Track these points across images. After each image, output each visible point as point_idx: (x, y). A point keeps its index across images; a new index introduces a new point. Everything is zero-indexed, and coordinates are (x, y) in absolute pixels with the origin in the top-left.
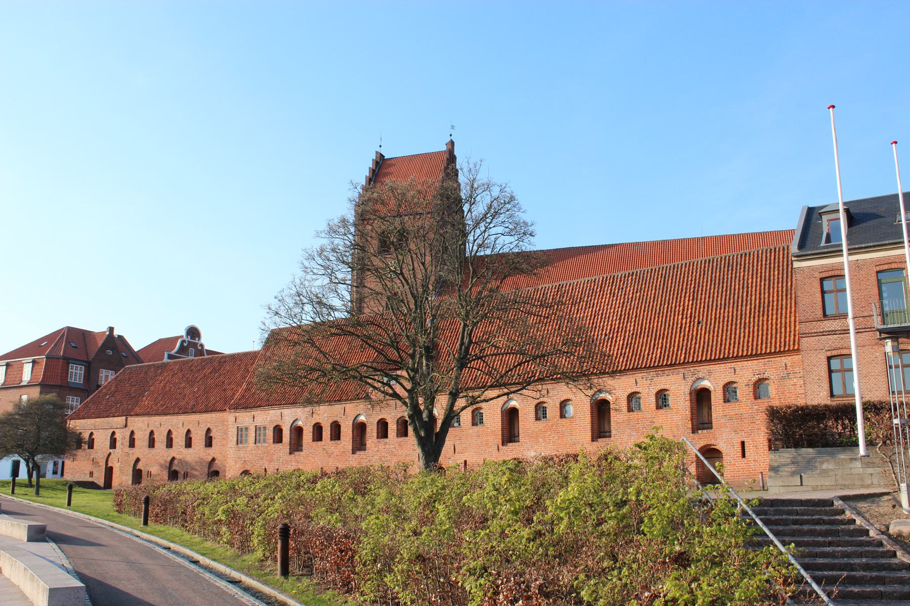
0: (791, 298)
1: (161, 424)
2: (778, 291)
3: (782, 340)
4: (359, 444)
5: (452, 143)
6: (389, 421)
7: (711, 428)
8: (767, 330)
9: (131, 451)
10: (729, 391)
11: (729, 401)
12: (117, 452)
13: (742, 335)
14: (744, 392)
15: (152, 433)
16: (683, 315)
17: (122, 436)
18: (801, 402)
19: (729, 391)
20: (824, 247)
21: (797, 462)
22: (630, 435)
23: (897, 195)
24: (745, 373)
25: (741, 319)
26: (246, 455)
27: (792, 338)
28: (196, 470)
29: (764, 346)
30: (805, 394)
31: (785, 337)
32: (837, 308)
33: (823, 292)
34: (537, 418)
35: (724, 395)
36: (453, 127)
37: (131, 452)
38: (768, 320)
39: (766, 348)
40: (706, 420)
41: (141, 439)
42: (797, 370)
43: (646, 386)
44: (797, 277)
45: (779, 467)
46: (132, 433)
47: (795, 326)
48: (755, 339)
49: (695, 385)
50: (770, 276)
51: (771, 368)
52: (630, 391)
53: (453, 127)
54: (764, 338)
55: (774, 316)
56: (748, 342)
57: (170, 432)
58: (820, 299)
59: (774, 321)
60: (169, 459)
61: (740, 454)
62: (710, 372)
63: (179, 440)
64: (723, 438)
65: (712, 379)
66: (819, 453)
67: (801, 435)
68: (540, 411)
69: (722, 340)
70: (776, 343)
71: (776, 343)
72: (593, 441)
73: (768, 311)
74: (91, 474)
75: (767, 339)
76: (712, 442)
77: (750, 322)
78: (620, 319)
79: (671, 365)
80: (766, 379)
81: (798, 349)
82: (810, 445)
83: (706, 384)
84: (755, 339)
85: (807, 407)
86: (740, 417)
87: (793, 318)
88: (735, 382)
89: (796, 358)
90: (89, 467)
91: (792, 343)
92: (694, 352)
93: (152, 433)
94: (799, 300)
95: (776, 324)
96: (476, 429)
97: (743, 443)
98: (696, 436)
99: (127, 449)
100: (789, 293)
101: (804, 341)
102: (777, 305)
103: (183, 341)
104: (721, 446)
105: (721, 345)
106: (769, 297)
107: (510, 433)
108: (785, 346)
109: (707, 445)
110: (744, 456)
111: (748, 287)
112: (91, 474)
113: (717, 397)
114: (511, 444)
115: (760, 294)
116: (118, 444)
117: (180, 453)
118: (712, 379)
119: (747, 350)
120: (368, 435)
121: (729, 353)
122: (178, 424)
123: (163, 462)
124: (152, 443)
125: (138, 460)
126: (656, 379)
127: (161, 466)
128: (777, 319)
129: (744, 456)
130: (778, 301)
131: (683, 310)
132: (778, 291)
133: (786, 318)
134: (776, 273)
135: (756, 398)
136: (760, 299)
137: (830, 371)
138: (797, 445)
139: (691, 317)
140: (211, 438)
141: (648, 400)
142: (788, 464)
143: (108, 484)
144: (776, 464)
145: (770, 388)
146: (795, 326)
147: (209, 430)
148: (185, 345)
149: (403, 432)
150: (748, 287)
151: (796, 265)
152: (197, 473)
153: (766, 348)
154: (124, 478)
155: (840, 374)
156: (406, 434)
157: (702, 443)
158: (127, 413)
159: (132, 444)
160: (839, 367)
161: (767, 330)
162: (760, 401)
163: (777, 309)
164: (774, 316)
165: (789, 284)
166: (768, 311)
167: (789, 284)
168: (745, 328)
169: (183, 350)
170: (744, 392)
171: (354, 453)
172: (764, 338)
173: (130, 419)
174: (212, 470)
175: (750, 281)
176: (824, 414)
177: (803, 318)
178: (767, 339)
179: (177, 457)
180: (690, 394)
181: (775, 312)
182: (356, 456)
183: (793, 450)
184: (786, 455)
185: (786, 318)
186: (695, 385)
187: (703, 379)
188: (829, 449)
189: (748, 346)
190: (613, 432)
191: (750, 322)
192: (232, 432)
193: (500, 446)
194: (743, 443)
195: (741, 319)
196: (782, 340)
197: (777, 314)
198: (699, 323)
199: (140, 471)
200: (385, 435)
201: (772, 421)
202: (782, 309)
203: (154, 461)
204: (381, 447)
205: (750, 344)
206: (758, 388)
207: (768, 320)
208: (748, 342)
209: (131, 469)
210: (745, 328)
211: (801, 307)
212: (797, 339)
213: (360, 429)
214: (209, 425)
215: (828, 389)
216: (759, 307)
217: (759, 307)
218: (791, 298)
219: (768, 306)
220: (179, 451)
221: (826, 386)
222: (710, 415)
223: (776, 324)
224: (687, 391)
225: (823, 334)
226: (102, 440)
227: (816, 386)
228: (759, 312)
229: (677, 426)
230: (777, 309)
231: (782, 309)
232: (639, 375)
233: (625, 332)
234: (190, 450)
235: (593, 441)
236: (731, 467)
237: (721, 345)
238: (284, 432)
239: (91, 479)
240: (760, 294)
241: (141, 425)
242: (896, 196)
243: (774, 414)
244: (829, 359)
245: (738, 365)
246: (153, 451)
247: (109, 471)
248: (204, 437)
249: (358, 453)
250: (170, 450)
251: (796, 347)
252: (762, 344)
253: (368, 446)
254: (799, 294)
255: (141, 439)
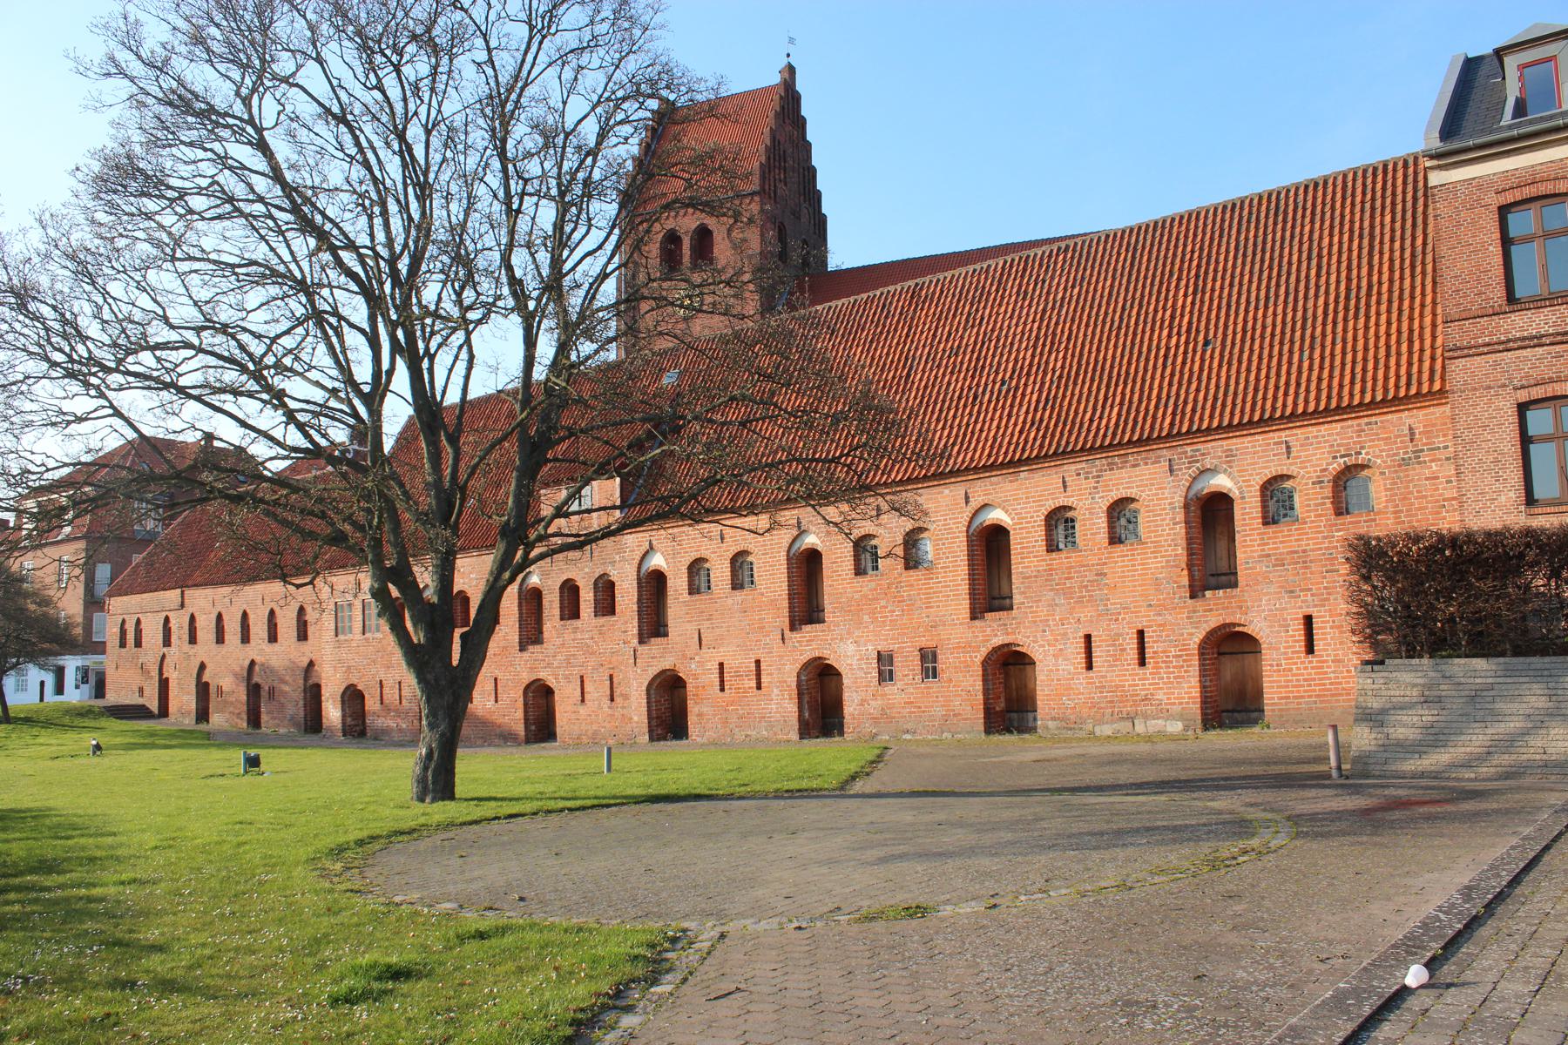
0: (1424, 273)
2: (1391, 260)
3: (1403, 371)
5: (791, 70)
6: (580, 583)
7: (1235, 585)
8: (1366, 349)
9: (192, 650)
10: (1276, 499)
11: (1275, 522)
12: (173, 652)
13: (1306, 365)
14: (1310, 499)
15: (220, 617)
16: (1171, 327)
17: (179, 623)
18: (1449, 523)
19: (1276, 499)
20: (1510, 127)
21: (1439, 700)
22: (1053, 605)
24: (1312, 453)
25: (1303, 328)
26: (350, 656)
27: (1426, 365)
28: (286, 682)
29: (1358, 387)
30: (1460, 499)
31: (1410, 364)
32: (1546, 279)
33: (1506, 242)
34: (859, 571)
35: (1264, 506)
36: (792, 41)
38: (1367, 328)
39: (1363, 392)
40: (1223, 565)
42: (1439, 441)
43: (1087, 490)
44: (1440, 207)
45: (1383, 711)
46: (192, 618)
47: (1434, 338)
48: (1337, 373)
49: (1197, 487)
50: (1372, 227)
51: (1376, 440)
52: (1051, 504)
53: (792, 41)
54: (1359, 368)
55: (1383, 318)
56: (1320, 379)
57: (245, 615)
58: (1497, 259)
59: (1383, 329)
60: (247, 663)
61: (1300, 646)
62: (1230, 455)
64: (1262, 609)
65: (1236, 470)
66: (1509, 672)
67: (1451, 620)
68: (864, 554)
69: (1257, 379)
70: (1386, 378)
71: (1386, 378)
72: (973, 618)
73: (1368, 306)
74: (141, 690)
75: (1364, 370)
76: (1237, 618)
77: (1324, 335)
78: (1035, 347)
79: (1140, 442)
80: (1363, 467)
81: (1442, 391)
82: (1481, 647)
83: (1221, 482)
84: (1337, 373)
85: (1470, 537)
86: (1301, 559)
87: (1428, 320)
88: (1289, 477)
89: (1438, 412)
90: (136, 680)
91: (1425, 376)
92: (1194, 410)
93: (220, 617)
94: (1444, 264)
95: (1388, 335)
96: (739, 596)
97: (1308, 620)
98: (1198, 604)
99: (186, 647)
100: (1421, 262)
101: (1460, 371)
102: (1390, 291)
104: (1256, 626)
105: (1256, 390)
106: (1370, 275)
107: (806, 605)
108: (1408, 384)
109: (1224, 626)
110: (1310, 649)
111: (1320, 256)
112: (141, 690)
113: (1247, 513)
114: (808, 628)
115: (1349, 269)
116: (174, 638)
118: (1236, 470)
119: (1318, 399)
120: (546, 613)
121: (1274, 409)
123: (237, 669)
125: (202, 667)
126: (1107, 475)
127: (236, 675)
128: (1389, 323)
129: (1310, 649)
130: (1391, 281)
131: (1172, 317)
132: (1391, 260)
133: (1411, 319)
134: (1388, 219)
135: (1339, 512)
136: (1349, 279)
137: (1526, 441)
138: (1440, 645)
139: (1188, 331)
141: (1092, 524)
142: (1411, 706)
143: (164, 712)
144: (1375, 704)
145: (1372, 487)
146: (1434, 338)
150: (1320, 256)
151: (1435, 178)
152: (287, 688)
153: (1363, 392)
154: (185, 698)
155: (1552, 446)
157: (1213, 621)
158: (183, 584)
159: (193, 639)
160: (1549, 429)
161: (1366, 349)
162: (1348, 518)
163: (1390, 301)
164: (1383, 318)
165: (1419, 241)
166: (1368, 306)
167: (1419, 241)
168: (1312, 348)
170: (1310, 499)
171: (522, 649)
172: (1359, 368)
173: (188, 592)
174: (311, 682)
175: (1326, 241)
176: (1521, 556)
177: (1454, 312)
178: (1364, 370)
179: (258, 659)
180: (1186, 506)
181: (1383, 308)
182: (526, 655)
183: (1425, 661)
184: (1407, 677)
185: (1411, 319)
186: (1197, 487)
187: (1213, 471)
188: (1537, 661)
189: (1319, 390)
190: (1017, 599)
191: (1324, 335)
193: (787, 632)
194: (1308, 620)
195: (1303, 328)
196: (1403, 371)
197: (1389, 311)
198: (1206, 343)
199: (207, 684)
200: (575, 615)
201: (1367, 578)
202: (1401, 299)
203: (227, 666)
204: (568, 636)
205: (1324, 384)
206: (1345, 484)
207: (1367, 328)
208: (1320, 379)
209: (194, 683)
210: (1312, 348)
211: (1447, 285)
212: (1438, 366)
215: (1520, 485)
216: (1347, 298)
217: (1347, 298)
218: (1424, 273)
219: (1369, 295)
220: (259, 648)
221: (1515, 476)
222: (1232, 554)
223: (1388, 335)
224: (1179, 500)
225: (1506, 346)
227: (1489, 479)
228: (1346, 309)
229: (1157, 583)
230: (1390, 301)
231: (1401, 299)
232: (1070, 469)
233: (1045, 373)
234: (276, 647)
235: (973, 618)
236: (1282, 675)
237: (1256, 390)
238: (582, 593)
239: (140, 701)
240: (1349, 269)
241: (205, 602)
243: (1370, 558)
244: (1522, 408)
245: (1297, 436)
247: (164, 685)
249: (531, 648)
250: (248, 647)
251: (1437, 386)
252: (1352, 383)
253: (546, 635)
254: (1443, 250)
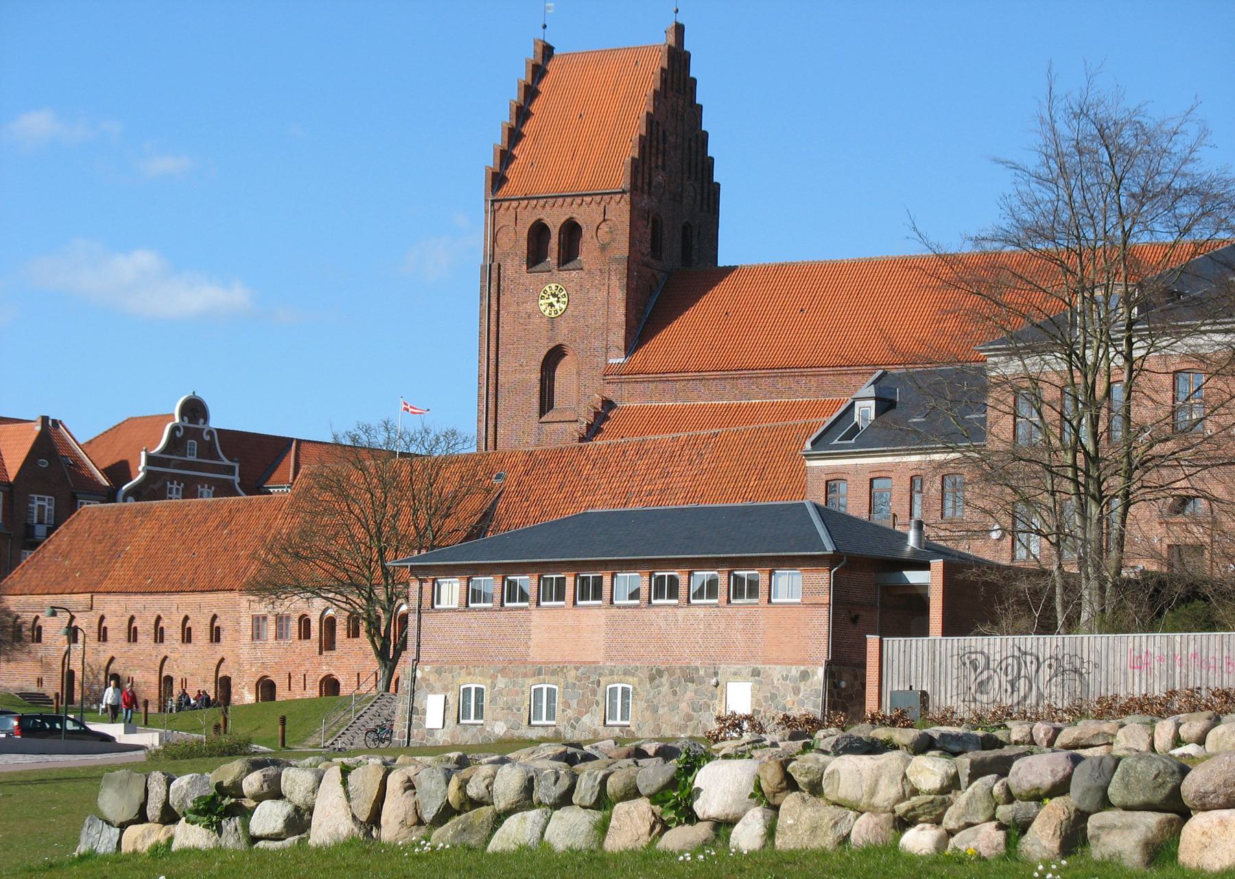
1: (146, 608)
4: (328, 643)
5: (679, 30)
23: (947, 631)
37: (102, 648)
41: (116, 627)
63: (173, 632)
74: (40, 681)
103: (175, 429)
112: (40, 681)
117: (174, 650)
122: (173, 608)
124: (132, 635)
140: (218, 628)
147: (159, 618)
148: (179, 434)
149: (354, 633)
156: (356, 635)
169: (175, 443)
174: (220, 675)
192: (246, 623)
213: (329, 625)
214: (215, 611)
226: (54, 629)
241: (115, 609)
242: (947, 631)
246: (135, 647)
248: (208, 627)
250: (217, 647)
255: (116, 627)
